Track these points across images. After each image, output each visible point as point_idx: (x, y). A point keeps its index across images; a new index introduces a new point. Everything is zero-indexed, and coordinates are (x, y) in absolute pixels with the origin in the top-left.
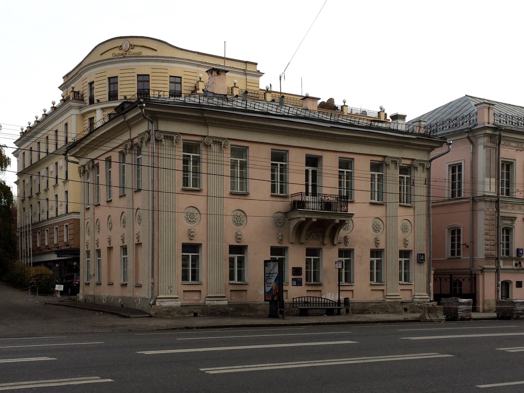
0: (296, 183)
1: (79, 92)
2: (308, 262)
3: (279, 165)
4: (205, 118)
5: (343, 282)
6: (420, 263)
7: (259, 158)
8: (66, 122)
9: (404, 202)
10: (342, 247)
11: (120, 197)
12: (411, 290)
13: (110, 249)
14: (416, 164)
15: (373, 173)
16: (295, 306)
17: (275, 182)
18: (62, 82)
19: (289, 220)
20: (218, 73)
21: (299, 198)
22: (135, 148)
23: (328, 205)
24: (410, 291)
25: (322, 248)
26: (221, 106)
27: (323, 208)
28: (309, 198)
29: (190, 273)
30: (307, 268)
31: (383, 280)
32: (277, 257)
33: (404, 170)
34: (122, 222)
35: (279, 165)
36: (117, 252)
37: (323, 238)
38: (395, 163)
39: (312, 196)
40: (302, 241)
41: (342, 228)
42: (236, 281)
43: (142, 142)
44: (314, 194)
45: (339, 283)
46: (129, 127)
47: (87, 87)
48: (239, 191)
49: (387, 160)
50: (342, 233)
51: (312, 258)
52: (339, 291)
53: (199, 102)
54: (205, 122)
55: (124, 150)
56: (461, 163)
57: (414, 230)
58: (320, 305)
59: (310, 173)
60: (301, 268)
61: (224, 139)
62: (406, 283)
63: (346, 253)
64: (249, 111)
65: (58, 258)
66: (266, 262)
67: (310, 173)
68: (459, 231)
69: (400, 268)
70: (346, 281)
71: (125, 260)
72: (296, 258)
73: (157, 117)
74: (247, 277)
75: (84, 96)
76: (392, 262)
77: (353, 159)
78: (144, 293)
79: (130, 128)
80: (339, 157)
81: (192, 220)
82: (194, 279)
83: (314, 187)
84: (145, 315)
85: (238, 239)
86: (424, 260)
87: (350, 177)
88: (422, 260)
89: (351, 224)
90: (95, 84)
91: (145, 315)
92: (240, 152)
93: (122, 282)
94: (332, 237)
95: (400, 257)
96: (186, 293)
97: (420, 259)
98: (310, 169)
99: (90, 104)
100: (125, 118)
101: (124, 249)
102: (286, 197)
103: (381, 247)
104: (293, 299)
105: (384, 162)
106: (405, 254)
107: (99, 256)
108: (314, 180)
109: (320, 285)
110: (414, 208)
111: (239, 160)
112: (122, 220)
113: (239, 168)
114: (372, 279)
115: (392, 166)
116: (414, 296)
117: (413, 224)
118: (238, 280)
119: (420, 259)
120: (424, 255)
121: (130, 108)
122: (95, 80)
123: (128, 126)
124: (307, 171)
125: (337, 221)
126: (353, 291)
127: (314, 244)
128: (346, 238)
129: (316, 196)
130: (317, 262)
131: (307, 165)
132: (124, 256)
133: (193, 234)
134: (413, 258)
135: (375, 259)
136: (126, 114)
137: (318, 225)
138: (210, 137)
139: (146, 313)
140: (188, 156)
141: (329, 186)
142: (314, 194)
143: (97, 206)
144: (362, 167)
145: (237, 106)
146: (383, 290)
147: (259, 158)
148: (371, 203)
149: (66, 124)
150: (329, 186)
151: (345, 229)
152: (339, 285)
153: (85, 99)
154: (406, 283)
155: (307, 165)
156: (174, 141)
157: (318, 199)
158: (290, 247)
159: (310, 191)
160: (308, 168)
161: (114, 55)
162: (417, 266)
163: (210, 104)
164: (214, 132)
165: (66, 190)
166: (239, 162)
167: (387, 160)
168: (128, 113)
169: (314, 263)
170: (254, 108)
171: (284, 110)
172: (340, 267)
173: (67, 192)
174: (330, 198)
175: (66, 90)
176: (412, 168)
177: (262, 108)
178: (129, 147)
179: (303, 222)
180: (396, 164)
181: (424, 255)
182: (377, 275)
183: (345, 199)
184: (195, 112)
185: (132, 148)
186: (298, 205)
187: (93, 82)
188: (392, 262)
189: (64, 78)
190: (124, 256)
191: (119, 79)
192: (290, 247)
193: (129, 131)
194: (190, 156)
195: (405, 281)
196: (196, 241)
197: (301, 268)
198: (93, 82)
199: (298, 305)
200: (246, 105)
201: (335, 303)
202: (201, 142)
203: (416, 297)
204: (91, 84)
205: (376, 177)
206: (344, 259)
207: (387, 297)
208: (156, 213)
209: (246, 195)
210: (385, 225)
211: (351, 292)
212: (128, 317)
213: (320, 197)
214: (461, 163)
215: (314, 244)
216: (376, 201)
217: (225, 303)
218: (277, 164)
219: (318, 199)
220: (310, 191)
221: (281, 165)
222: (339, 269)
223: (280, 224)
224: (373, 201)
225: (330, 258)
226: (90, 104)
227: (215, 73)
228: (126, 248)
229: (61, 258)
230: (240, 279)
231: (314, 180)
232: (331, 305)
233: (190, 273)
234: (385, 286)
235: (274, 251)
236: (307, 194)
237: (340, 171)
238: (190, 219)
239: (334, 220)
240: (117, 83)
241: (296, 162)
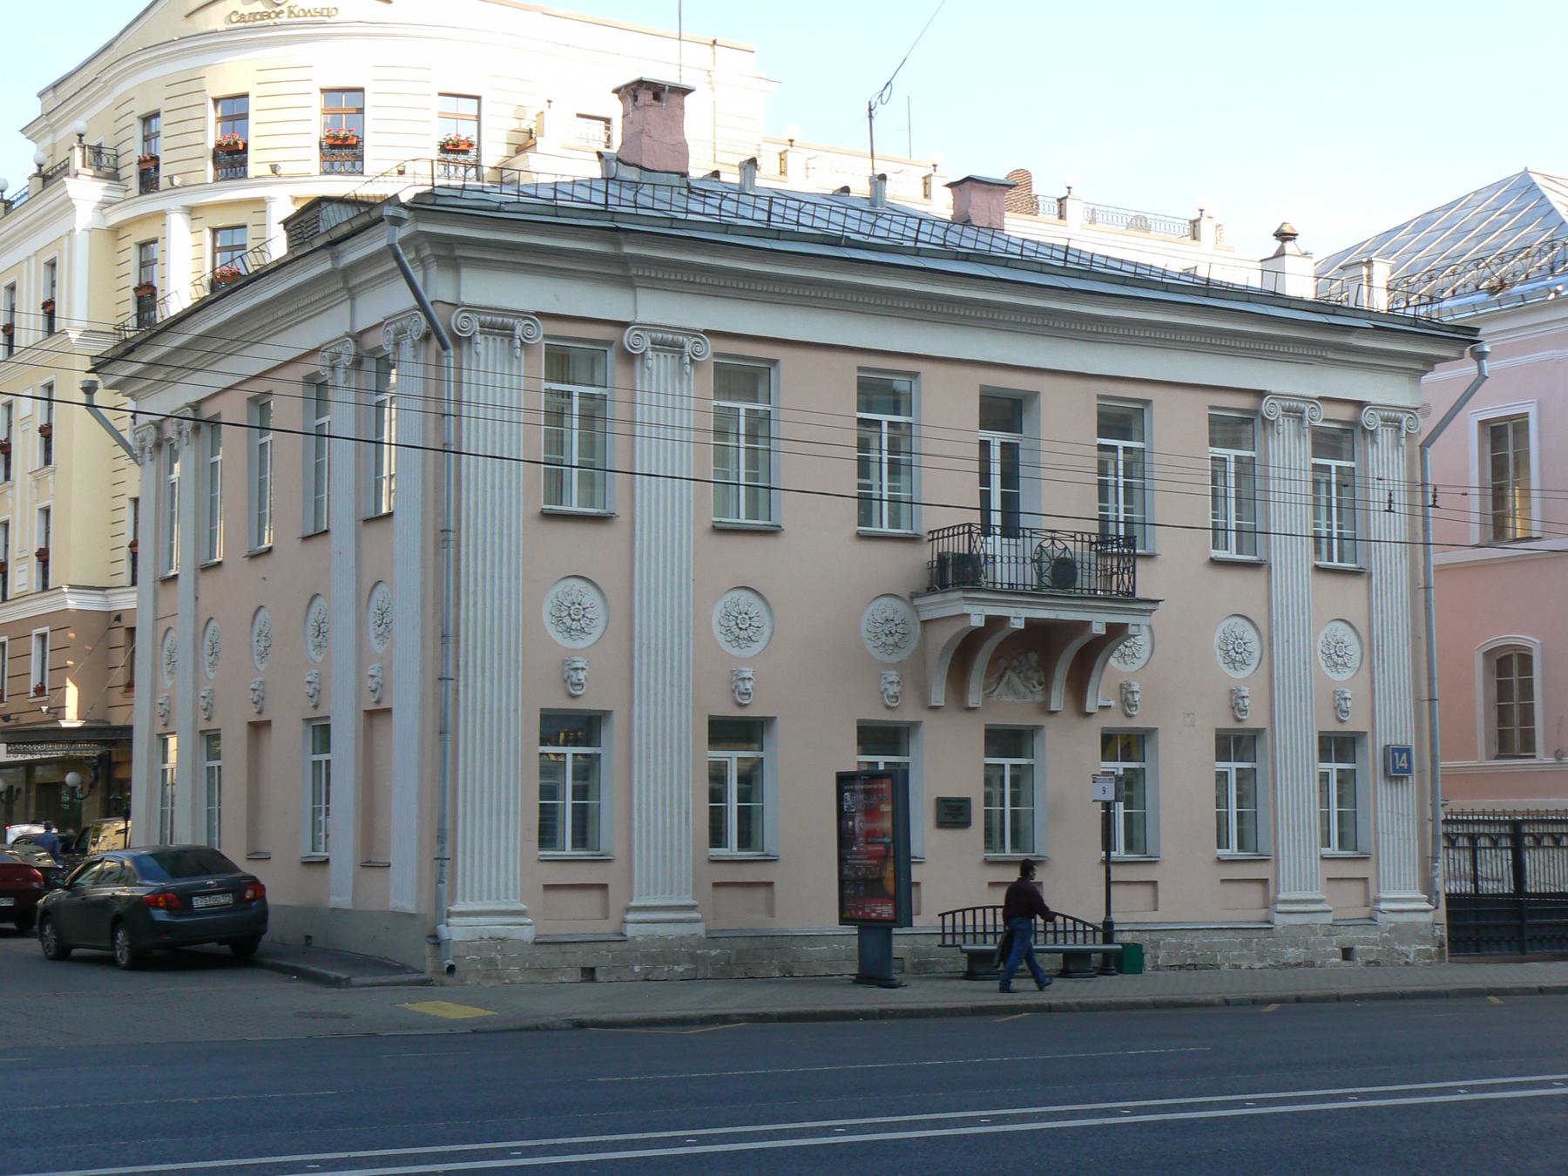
0: (947, 490)
1: (99, 146)
2: (992, 776)
3: (885, 425)
4: (623, 261)
5: (1119, 852)
6: (1391, 778)
7: (815, 407)
8: (48, 258)
9: (1330, 559)
10: (1115, 721)
11: (306, 538)
12: (1365, 879)
13: (258, 728)
14: (1369, 419)
15: (1220, 452)
16: (949, 941)
17: (869, 487)
18: (34, 109)
19: (925, 623)
20: (657, 97)
21: (958, 545)
22: (370, 365)
23: (1062, 575)
24: (1360, 885)
25: (1041, 727)
26: (683, 216)
27: (1046, 580)
28: (995, 545)
29: (568, 817)
30: (988, 799)
31: (605, 845)
32: (882, 761)
33: (1330, 442)
34: (311, 631)
35: (885, 425)
36: (288, 741)
37: (1047, 685)
38: (1297, 415)
39: (1003, 535)
40: (974, 698)
41: (1111, 654)
42: (732, 849)
43: (397, 344)
44: (1011, 529)
45: (1108, 855)
46: (350, 290)
47: (137, 131)
48: (743, 520)
49: (1266, 406)
50: (1116, 667)
51: (1008, 762)
52: (1109, 883)
53: (606, 204)
54: (623, 274)
55: (327, 373)
56: (1526, 415)
57: (1371, 661)
58: (980, 938)
59: (996, 454)
60: (967, 801)
61: (692, 333)
62: (746, 854)
63: (1126, 744)
64: (779, 235)
65: (12, 758)
66: (844, 780)
67: (996, 454)
68: (1526, 660)
69: (1325, 801)
70: (1129, 846)
71: (322, 774)
72: (947, 761)
73: (455, 258)
74: (773, 834)
75: (122, 161)
76: (1295, 772)
77: (1147, 402)
78: (403, 891)
79: (352, 294)
80: (1100, 397)
81: (575, 625)
82: (581, 839)
83: (1011, 506)
84: (406, 977)
85: (570, 684)
86: (1409, 770)
87: (1137, 468)
88: (1402, 770)
89: (1143, 639)
90: (165, 118)
91: (406, 977)
92: (744, 375)
93: (306, 851)
94: (1079, 685)
95: (1321, 761)
96: (553, 894)
97: (1397, 766)
98: (996, 438)
99: (141, 193)
100: (335, 258)
101: (321, 733)
102: (913, 539)
103: (1252, 721)
104: (943, 915)
105: (1256, 412)
106: (1338, 745)
107: (214, 755)
108: (1010, 477)
109: (771, 860)
110: (1370, 576)
111: (743, 407)
112: (311, 621)
113: (742, 439)
114: (1222, 842)
115: (1287, 426)
116: (1378, 901)
117: (1364, 634)
118: (575, 845)
119: (1397, 766)
120: (1408, 751)
121: (356, 223)
122: (163, 106)
123: (347, 283)
124: (985, 446)
125: (1099, 629)
126: (1154, 883)
127: (1012, 710)
128: (1125, 693)
129: (1017, 537)
130: (1021, 777)
131: (984, 425)
132: (317, 758)
133: (749, 685)
134: (1369, 763)
135: (1232, 767)
136: (341, 247)
137: (1033, 640)
138: (643, 327)
139: (403, 968)
140: (562, 394)
141: (1063, 501)
142: (1011, 529)
143: (207, 568)
144: (1178, 438)
145: (737, 216)
146: (1265, 881)
147: (815, 407)
148: (1216, 563)
149: (52, 265)
150: (1063, 501)
151: (1123, 655)
152: (1107, 862)
153: (123, 173)
154: (746, 854)
155: (984, 425)
156: (518, 343)
157: (1028, 546)
158: (930, 723)
159: (996, 519)
160: (986, 435)
161: (234, 19)
162: (1384, 791)
163: (640, 211)
164: (658, 309)
165: (43, 504)
166: (742, 412)
167: (1266, 406)
168: (349, 243)
169: (1015, 782)
170: (798, 224)
171: (894, 227)
172: (1110, 796)
173: (46, 511)
174: (1070, 545)
175: (48, 141)
176: (1358, 433)
177: (824, 225)
178: (346, 360)
179: (978, 630)
180: (1301, 419)
181: (1408, 751)
182: (1242, 827)
183: (1121, 546)
184: (600, 240)
185: (358, 363)
186: (957, 572)
187: (157, 115)
188: (1295, 772)
189: (41, 95)
190: (317, 758)
191: (253, 104)
192: (927, 718)
193: (347, 306)
194: (569, 394)
195: (1341, 846)
196: (589, 702)
197: (967, 801)
198: (157, 115)
199: (959, 939)
200: (770, 213)
201: (1096, 929)
202: (609, 343)
203: (1383, 906)
204: (147, 119)
205: (1231, 467)
206: (1119, 767)
207: (1280, 907)
208: (1425, 695)
209: (772, 532)
210: (1265, 637)
211: (1148, 889)
212: (336, 983)
213: (1036, 542)
214: (1526, 415)
215: (1012, 710)
216: (1231, 554)
217: (700, 929)
218: (879, 423)
219: (1028, 546)
220: (996, 519)
221: (891, 424)
222: (1107, 806)
223: (890, 640)
224: (1221, 554)
225: (1070, 767)
226: (141, 193)
227: (646, 97)
228: (326, 729)
229: (20, 758)
230: (745, 841)
231: (1010, 477)
232: (1080, 936)
233: (568, 817)
234: (1372, 864)
235: (874, 736)
236: (986, 530)
237: (1101, 448)
238: (568, 621)
239: (1088, 623)
240: (245, 116)
241: (947, 419)
